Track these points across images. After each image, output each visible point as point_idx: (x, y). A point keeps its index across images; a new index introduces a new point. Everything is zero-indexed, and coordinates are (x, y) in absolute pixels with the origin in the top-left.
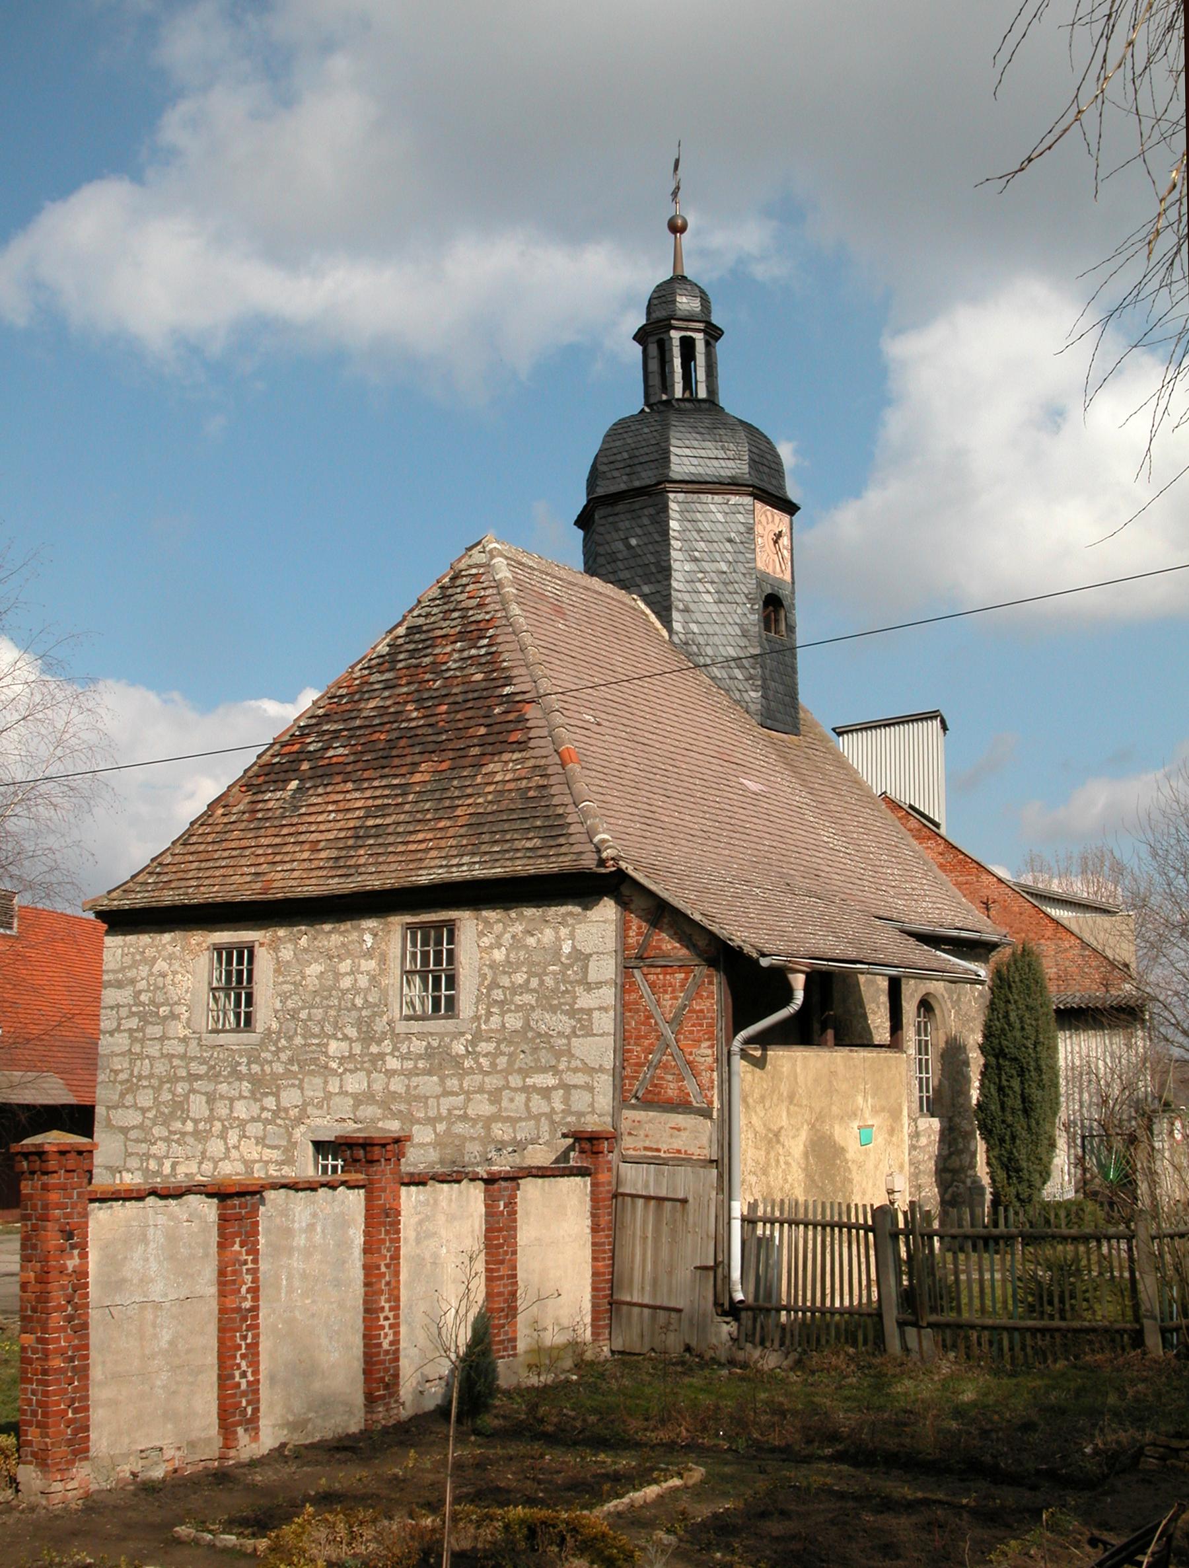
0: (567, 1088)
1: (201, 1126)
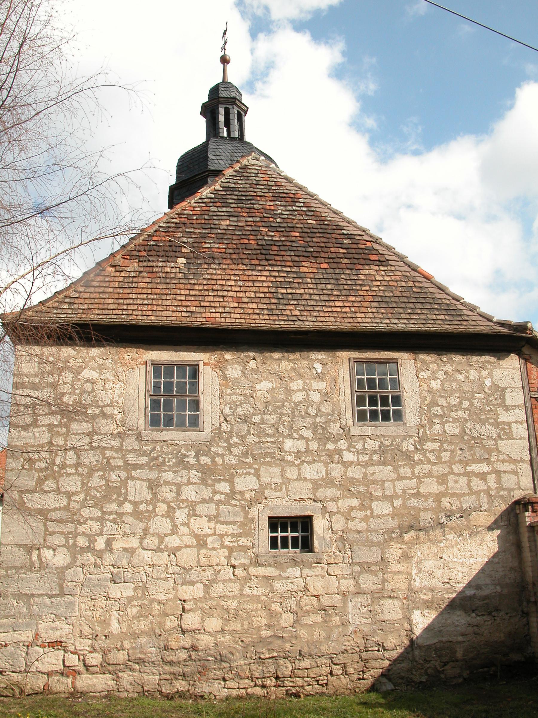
0: (498, 473)
1: (142, 507)
